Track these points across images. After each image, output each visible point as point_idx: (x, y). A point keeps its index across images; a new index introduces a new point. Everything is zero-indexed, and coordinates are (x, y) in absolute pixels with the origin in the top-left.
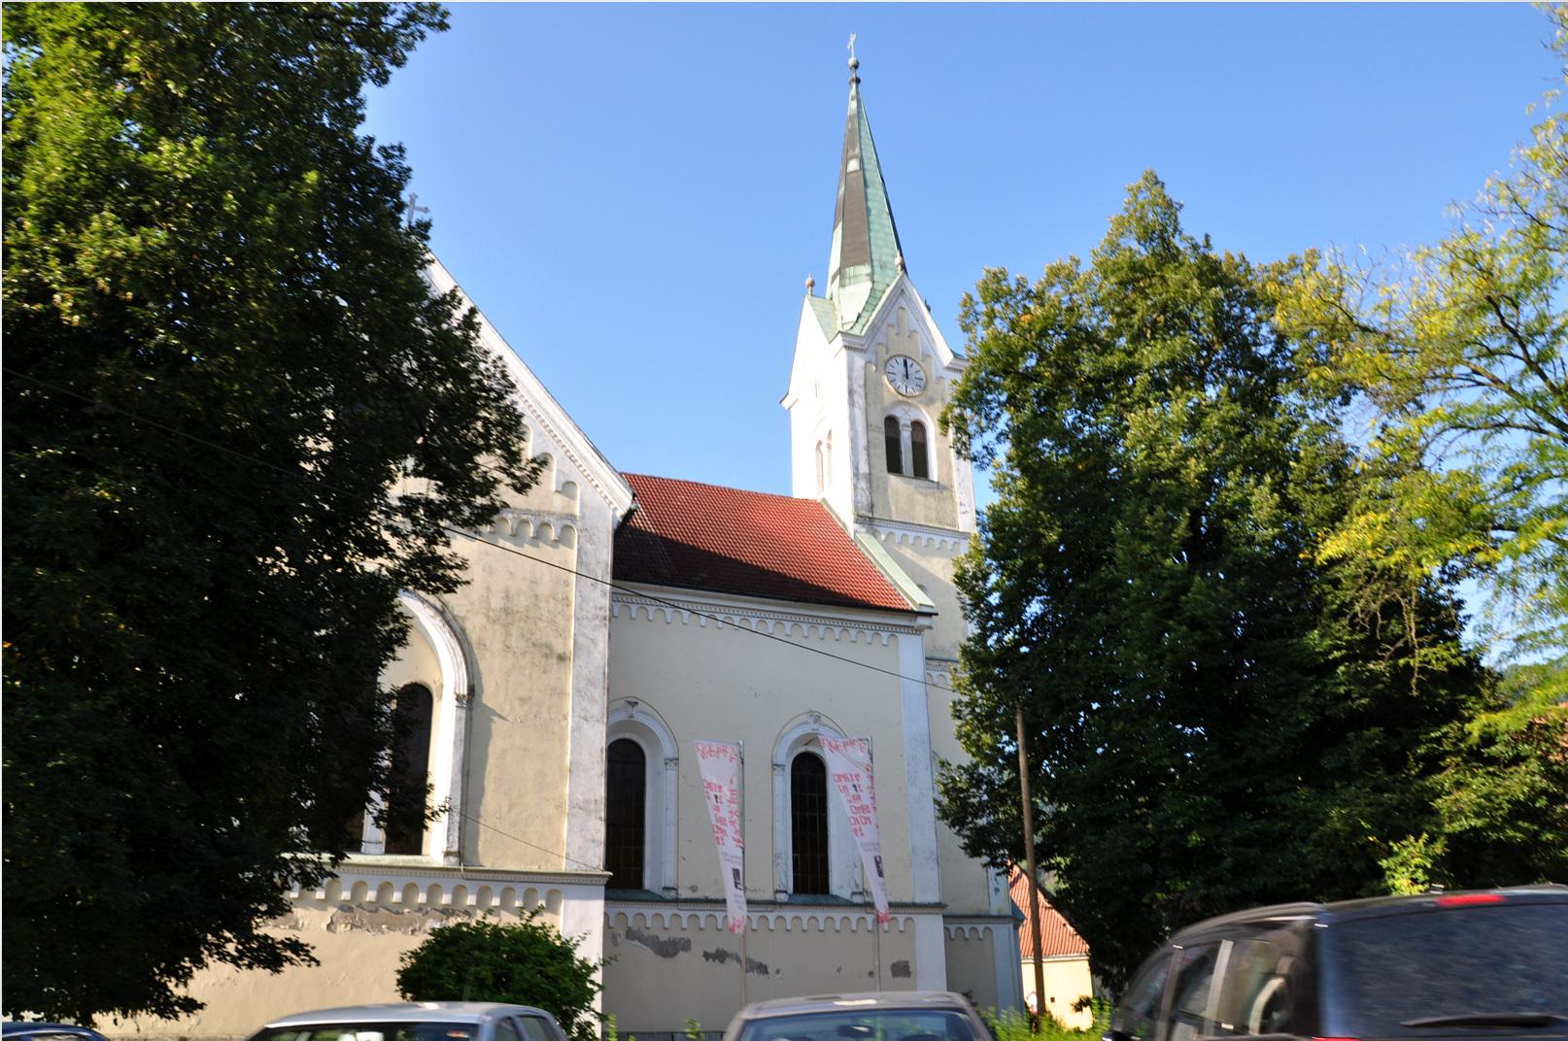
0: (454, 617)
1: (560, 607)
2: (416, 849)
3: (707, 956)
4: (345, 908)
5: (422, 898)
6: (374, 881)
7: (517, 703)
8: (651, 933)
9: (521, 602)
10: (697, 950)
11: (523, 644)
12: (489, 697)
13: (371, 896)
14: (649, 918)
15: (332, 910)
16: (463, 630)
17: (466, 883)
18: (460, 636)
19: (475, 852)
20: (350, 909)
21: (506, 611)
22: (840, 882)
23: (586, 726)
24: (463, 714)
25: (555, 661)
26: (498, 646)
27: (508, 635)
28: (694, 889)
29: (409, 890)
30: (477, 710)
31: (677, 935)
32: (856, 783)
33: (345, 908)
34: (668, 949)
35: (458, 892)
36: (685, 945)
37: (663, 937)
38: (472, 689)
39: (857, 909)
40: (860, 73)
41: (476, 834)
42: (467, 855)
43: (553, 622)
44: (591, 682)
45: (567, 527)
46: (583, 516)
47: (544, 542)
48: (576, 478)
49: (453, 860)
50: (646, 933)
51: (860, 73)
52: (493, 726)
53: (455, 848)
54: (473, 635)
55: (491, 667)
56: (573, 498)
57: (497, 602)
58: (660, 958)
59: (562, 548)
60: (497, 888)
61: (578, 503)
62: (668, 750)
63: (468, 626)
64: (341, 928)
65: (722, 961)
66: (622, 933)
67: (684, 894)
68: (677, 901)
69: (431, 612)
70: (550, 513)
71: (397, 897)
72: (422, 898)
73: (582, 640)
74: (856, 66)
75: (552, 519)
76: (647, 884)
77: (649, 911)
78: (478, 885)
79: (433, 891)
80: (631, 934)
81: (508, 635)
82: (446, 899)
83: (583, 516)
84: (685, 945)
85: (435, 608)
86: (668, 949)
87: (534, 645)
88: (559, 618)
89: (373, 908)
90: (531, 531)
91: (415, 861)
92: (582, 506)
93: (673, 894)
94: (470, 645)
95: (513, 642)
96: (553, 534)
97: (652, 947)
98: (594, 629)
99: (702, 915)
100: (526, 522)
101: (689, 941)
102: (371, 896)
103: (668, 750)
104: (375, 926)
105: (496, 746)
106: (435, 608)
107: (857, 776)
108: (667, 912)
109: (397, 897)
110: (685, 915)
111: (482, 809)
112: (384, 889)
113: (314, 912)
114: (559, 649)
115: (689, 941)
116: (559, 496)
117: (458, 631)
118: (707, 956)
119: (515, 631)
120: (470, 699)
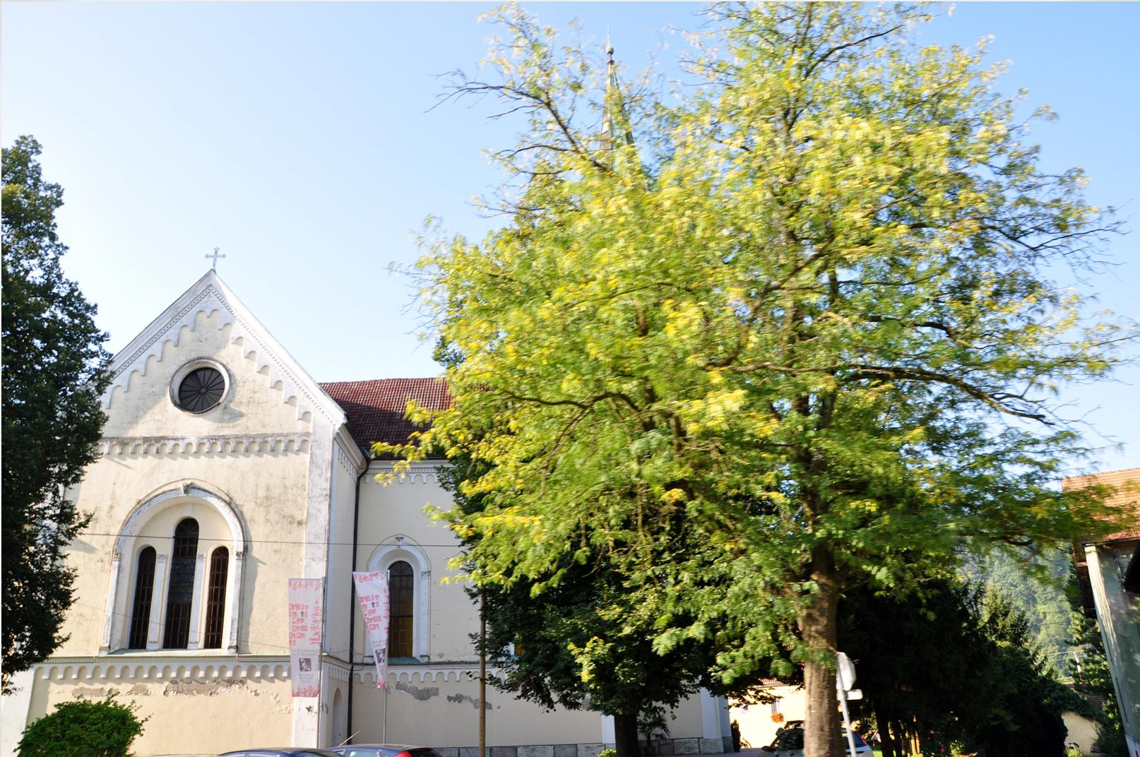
0: (236, 506)
1: (300, 492)
2: (218, 645)
3: (450, 698)
4: (174, 682)
5: (215, 674)
6: (189, 666)
7: (272, 554)
8: (413, 685)
9: (276, 492)
10: (443, 695)
11: (277, 517)
12: (257, 551)
13: (187, 674)
14: (422, 676)
15: (167, 683)
16: (242, 513)
17: (241, 664)
18: (239, 516)
19: (247, 646)
20: (176, 683)
21: (267, 498)
22: (419, 647)
23: (314, 564)
24: (240, 563)
25: (296, 525)
26: (262, 520)
27: (268, 512)
28: (441, 655)
29: (209, 670)
30: (249, 561)
31: (430, 685)
32: (375, 601)
33: (174, 682)
34: (424, 695)
35: (236, 670)
36: (435, 692)
37: (421, 687)
38: (246, 549)
39: (422, 667)
40: (614, 57)
41: (248, 634)
42: (242, 648)
43: (295, 501)
44: (317, 536)
45: (305, 441)
46: (315, 432)
47: (292, 452)
48: (312, 409)
49: (233, 650)
50: (409, 685)
51: (614, 57)
52: (259, 569)
53: (235, 644)
54: (247, 515)
55: (256, 533)
56: (309, 422)
57: (262, 493)
58: (418, 701)
59: (302, 454)
60: (259, 666)
61: (311, 425)
62: (424, 567)
63: (244, 510)
64: (171, 693)
65: (460, 702)
66: (394, 686)
67: (434, 659)
68: (428, 664)
69: (223, 504)
70: (294, 434)
71: (201, 674)
72: (215, 674)
73: (312, 511)
74: (611, 52)
75: (295, 437)
76: (416, 653)
77: (410, 671)
78: (248, 665)
79: (222, 670)
80: (399, 686)
81: (268, 512)
82: (229, 674)
83: (315, 432)
84: (435, 692)
85: (225, 501)
86: (424, 695)
87: (284, 517)
88: (299, 498)
89: (189, 681)
90: (282, 446)
91: (1100, 601)
92: (314, 426)
93: (426, 660)
94: (245, 521)
95: (271, 517)
96: (296, 446)
97: (413, 694)
98: (320, 503)
99: (446, 672)
100: (280, 441)
101: (437, 689)
102: (187, 674)
103: (424, 567)
104: (190, 692)
105: (259, 581)
106: (225, 501)
107: (377, 596)
108: (422, 671)
109: (201, 674)
110: (434, 673)
111: (251, 619)
112: (195, 670)
113: (157, 685)
114: (298, 518)
115: (437, 689)
116: (300, 422)
117: (239, 514)
118: (450, 698)
119: (272, 510)
120: (245, 553)
